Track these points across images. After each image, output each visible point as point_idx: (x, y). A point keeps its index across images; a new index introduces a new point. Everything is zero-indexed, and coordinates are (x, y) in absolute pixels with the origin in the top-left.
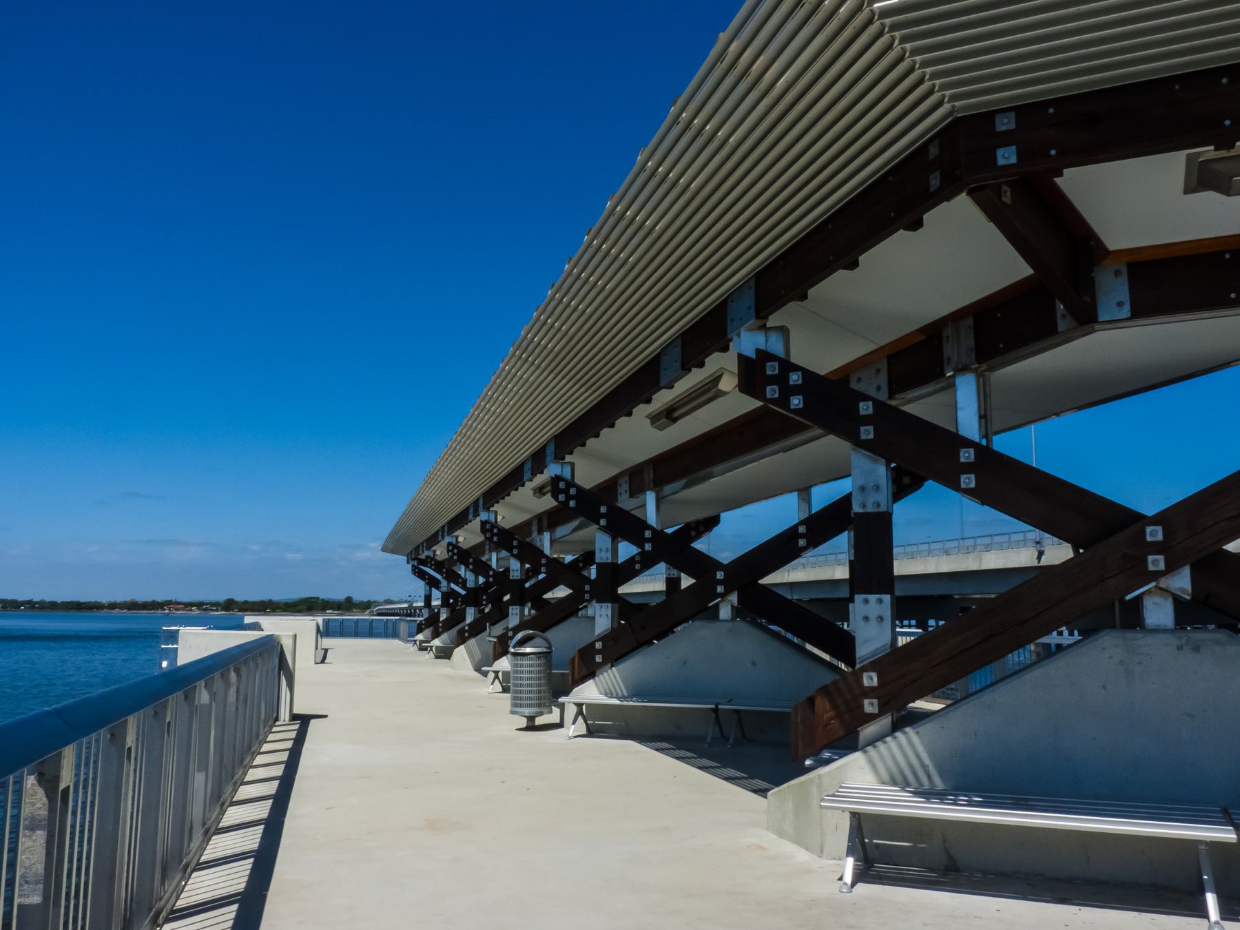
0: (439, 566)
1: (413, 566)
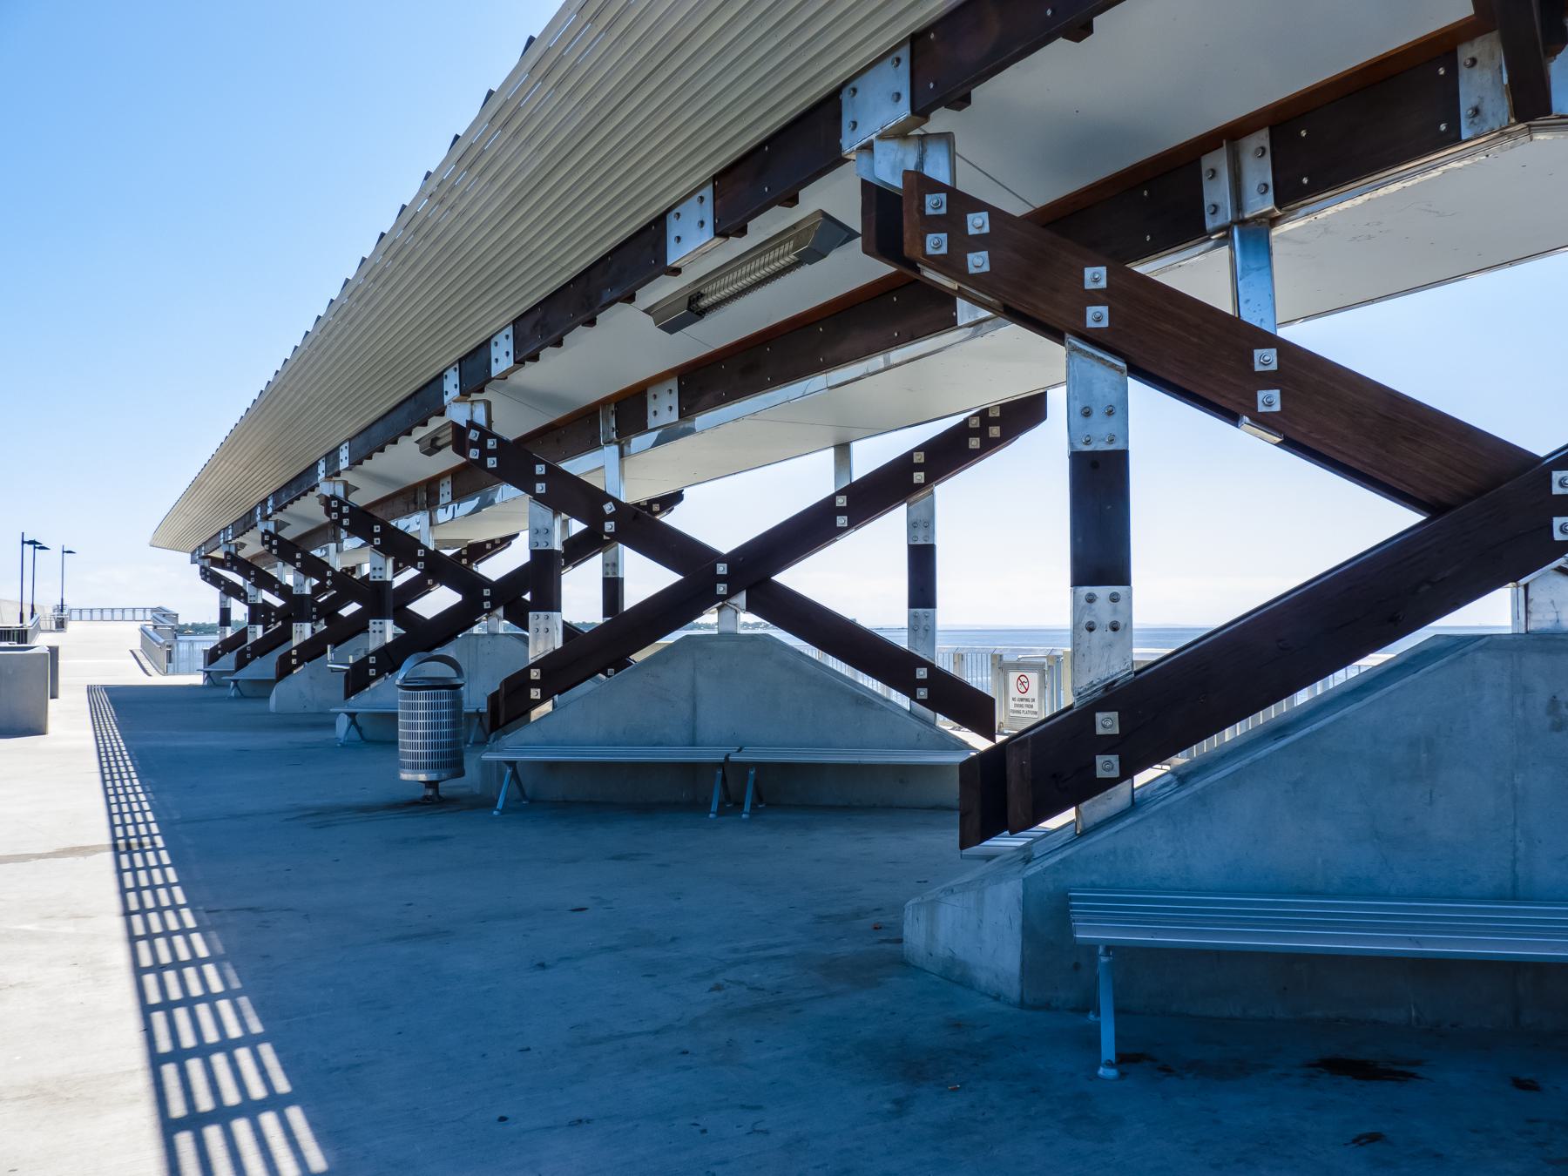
0: (243, 567)
1: (202, 567)
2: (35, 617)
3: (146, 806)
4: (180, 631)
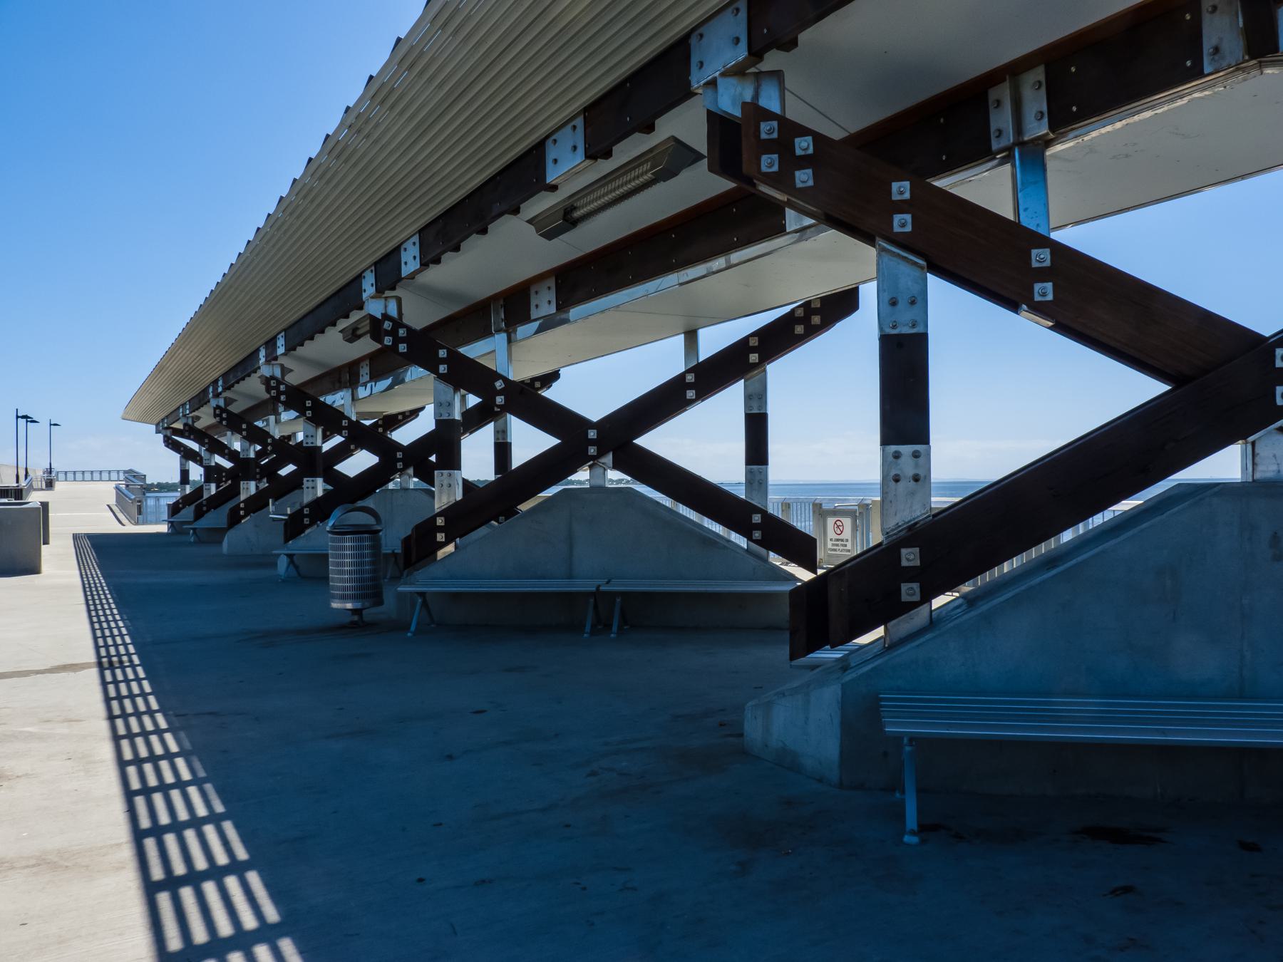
0: (198, 435)
1: (165, 436)
2: (29, 479)
3: (124, 631)
4: (148, 488)
